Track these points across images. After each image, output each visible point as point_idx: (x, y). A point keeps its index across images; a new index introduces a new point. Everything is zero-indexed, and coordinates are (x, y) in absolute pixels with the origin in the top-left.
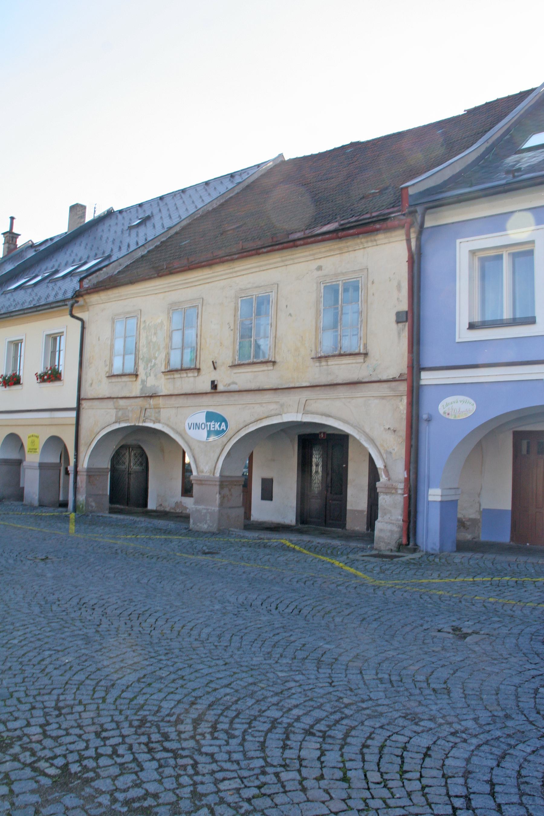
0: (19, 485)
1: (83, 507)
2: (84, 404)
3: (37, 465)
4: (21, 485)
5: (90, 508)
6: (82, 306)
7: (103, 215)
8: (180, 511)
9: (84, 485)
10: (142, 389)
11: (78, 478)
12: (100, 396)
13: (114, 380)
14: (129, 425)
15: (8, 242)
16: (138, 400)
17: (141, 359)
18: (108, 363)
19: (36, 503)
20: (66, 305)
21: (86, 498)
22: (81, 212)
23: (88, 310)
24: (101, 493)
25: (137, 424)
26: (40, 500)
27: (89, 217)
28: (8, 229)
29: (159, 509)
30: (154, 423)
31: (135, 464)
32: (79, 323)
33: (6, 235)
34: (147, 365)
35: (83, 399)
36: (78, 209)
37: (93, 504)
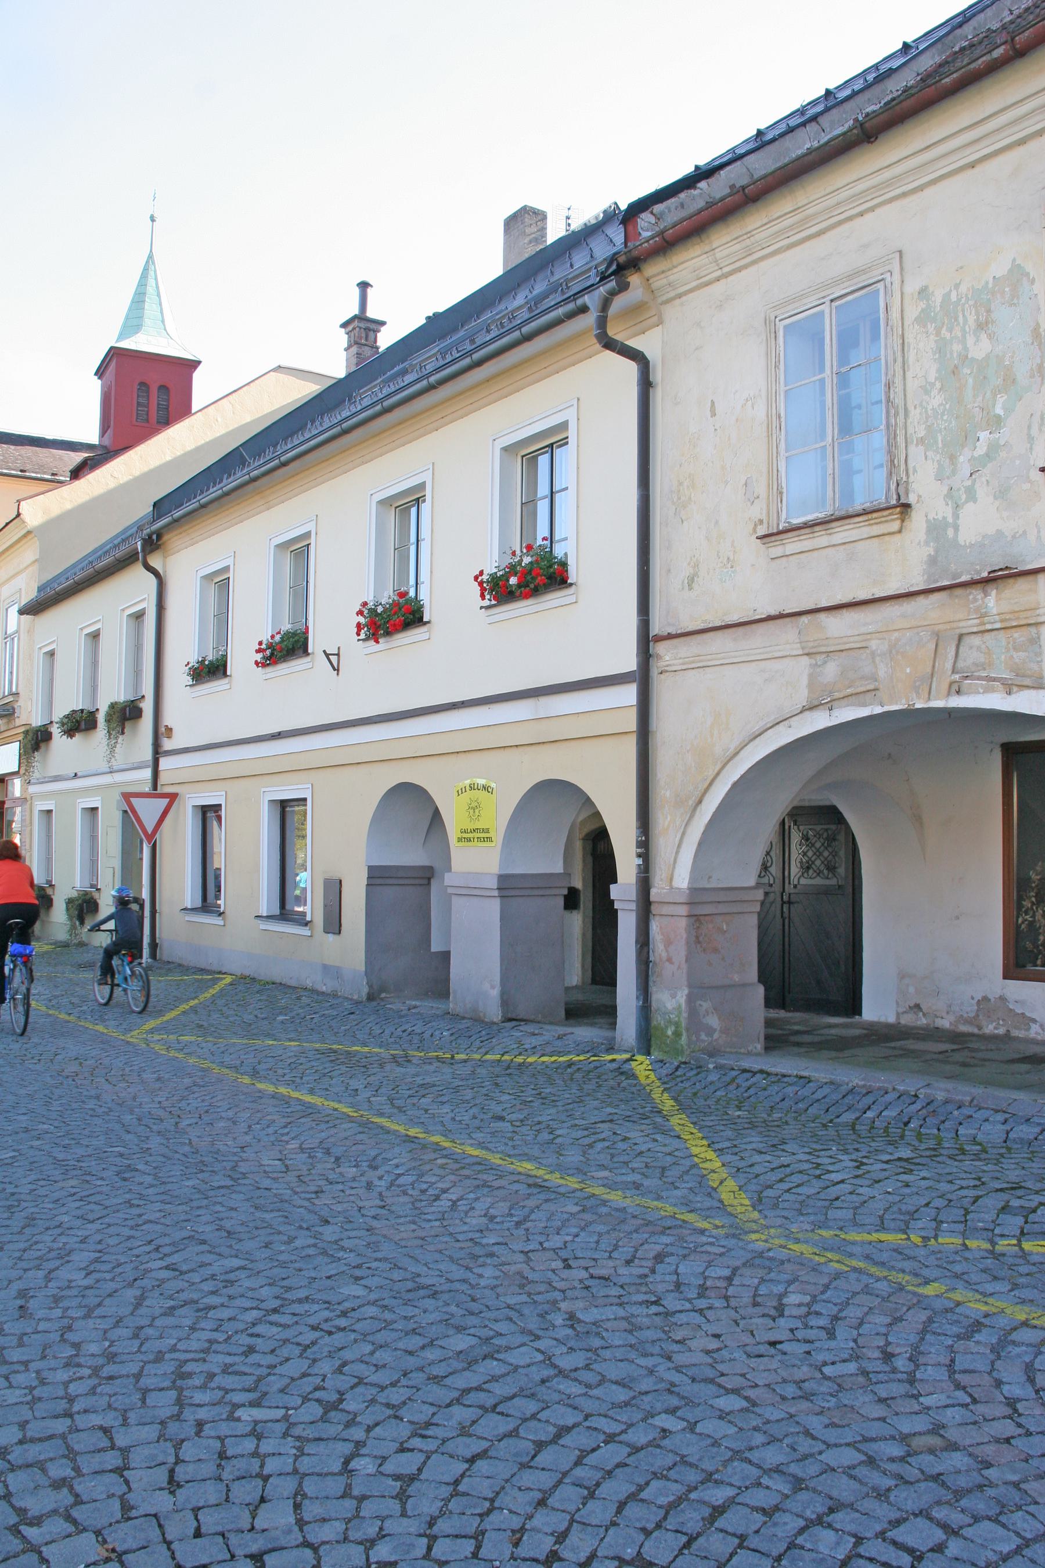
0: (426, 938)
1: (677, 1034)
2: (666, 654)
3: (494, 884)
4: (436, 946)
5: (703, 1037)
6: (637, 309)
7: (593, 222)
8: (1001, 1031)
9: (680, 952)
10: (933, 561)
11: (655, 926)
12: (735, 618)
13: (793, 545)
14: (878, 710)
15: (356, 343)
16: (922, 601)
17: (921, 441)
18: (761, 489)
19: (494, 1013)
20: (584, 309)
21: (690, 999)
22: (534, 229)
23: (660, 322)
24: (736, 978)
25: (919, 705)
26: (505, 1001)
27: (554, 232)
28: (356, 311)
29: (907, 1020)
30: (1009, 688)
31: (806, 867)
32: (631, 368)
33: (350, 328)
34: (953, 458)
35: (659, 639)
36: (527, 220)
37: (713, 1021)
